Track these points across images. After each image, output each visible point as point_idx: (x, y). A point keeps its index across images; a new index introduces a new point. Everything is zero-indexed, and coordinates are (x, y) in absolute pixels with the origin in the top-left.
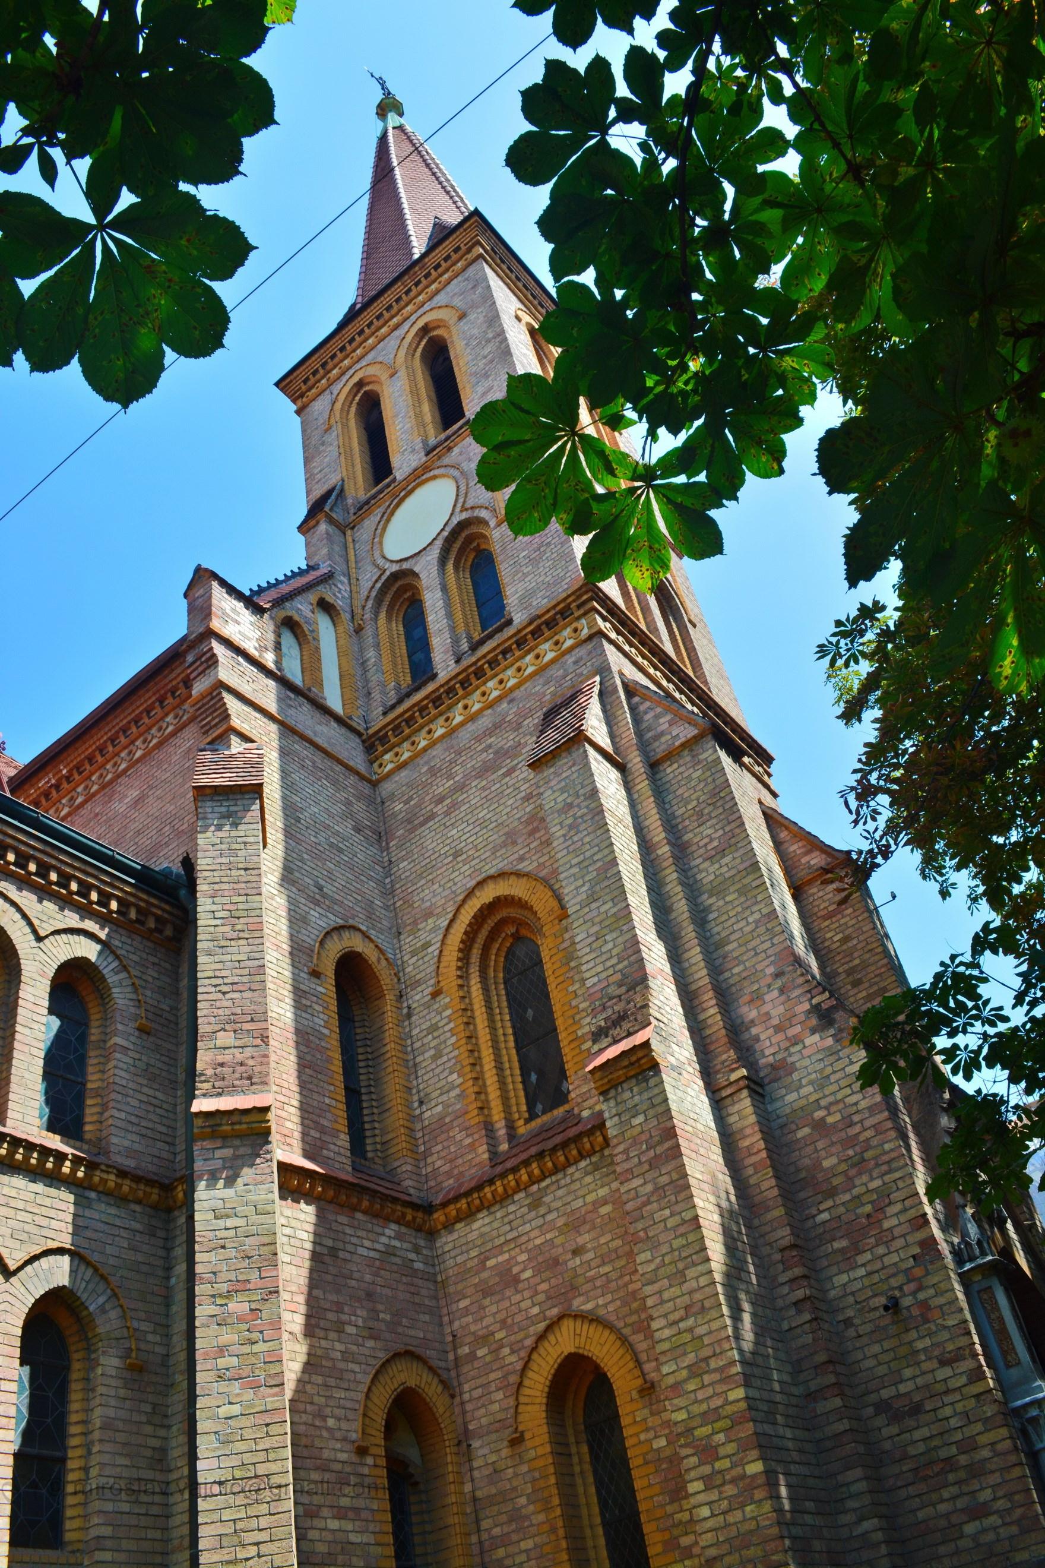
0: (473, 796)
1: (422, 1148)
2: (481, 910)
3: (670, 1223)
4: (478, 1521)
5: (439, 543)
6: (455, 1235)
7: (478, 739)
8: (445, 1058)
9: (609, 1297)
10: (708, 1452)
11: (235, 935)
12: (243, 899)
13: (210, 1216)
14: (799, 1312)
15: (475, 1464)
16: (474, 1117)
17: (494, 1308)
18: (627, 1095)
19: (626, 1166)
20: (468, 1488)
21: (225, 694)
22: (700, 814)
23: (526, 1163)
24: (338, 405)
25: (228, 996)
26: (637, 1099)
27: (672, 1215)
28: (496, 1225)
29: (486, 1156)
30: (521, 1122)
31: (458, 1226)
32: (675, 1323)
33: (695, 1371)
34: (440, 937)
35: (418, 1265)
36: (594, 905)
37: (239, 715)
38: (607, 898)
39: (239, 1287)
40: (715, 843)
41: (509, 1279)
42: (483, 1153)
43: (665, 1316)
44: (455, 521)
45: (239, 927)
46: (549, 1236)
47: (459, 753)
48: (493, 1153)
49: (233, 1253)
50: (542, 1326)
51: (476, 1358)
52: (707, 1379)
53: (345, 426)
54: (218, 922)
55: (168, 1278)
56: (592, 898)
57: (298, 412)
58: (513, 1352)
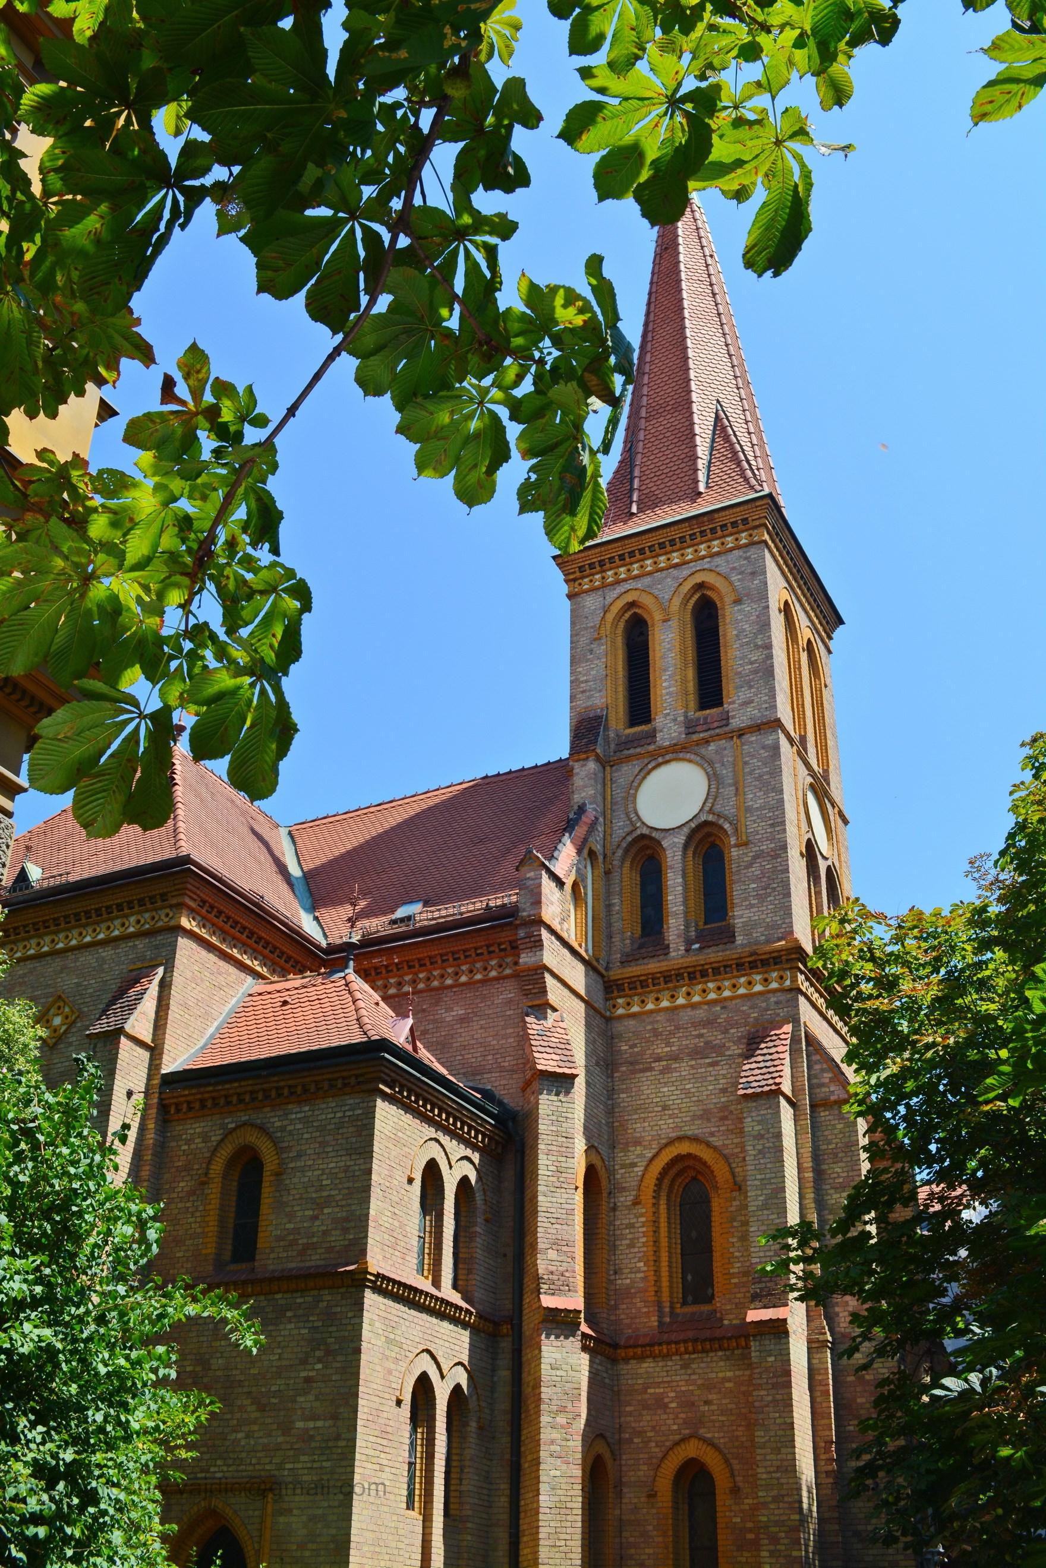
0: (684, 1068)
1: (613, 1303)
2: (676, 1157)
3: (778, 1421)
4: (621, 1532)
5: (686, 830)
6: (630, 1367)
7: (695, 1025)
8: (636, 1250)
9: (722, 1434)
10: (774, 1540)
11: (558, 1184)
12: (564, 1159)
13: (549, 1367)
14: (827, 1476)
15: (624, 1501)
16: (651, 1296)
17: (649, 1418)
18: (767, 1342)
19: (759, 1381)
20: (617, 1512)
21: (547, 976)
22: (836, 1155)
23: (685, 1341)
24: (610, 617)
25: (555, 1226)
26: (772, 1347)
27: (780, 1417)
28: (658, 1369)
29: (656, 1324)
30: (679, 1305)
31: (632, 1361)
32: (770, 1472)
33: (776, 1499)
34: (644, 1164)
35: (607, 1381)
36: (765, 1212)
37: (555, 992)
38: (775, 1211)
39: (562, 1410)
40: (841, 1180)
41: (660, 1404)
42: (654, 1321)
43: (766, 1467)
44: (703, 817)
45: (561, 1179)
46: (691, 1388)
47: (678, 1028)
48: (661, 1323)
49: (559, 1390)
50: (677, 1437)
51: (632, 1442)
52: (781, 1505)
53: (613, 642)
54: (550, 1173)
55: (493, 1376)
56: (765, 1207)
57: (570, 596)
58: (657, 1446)
